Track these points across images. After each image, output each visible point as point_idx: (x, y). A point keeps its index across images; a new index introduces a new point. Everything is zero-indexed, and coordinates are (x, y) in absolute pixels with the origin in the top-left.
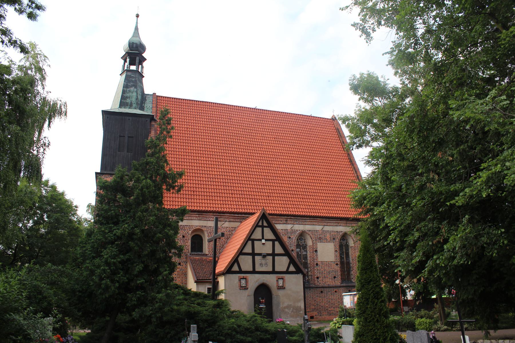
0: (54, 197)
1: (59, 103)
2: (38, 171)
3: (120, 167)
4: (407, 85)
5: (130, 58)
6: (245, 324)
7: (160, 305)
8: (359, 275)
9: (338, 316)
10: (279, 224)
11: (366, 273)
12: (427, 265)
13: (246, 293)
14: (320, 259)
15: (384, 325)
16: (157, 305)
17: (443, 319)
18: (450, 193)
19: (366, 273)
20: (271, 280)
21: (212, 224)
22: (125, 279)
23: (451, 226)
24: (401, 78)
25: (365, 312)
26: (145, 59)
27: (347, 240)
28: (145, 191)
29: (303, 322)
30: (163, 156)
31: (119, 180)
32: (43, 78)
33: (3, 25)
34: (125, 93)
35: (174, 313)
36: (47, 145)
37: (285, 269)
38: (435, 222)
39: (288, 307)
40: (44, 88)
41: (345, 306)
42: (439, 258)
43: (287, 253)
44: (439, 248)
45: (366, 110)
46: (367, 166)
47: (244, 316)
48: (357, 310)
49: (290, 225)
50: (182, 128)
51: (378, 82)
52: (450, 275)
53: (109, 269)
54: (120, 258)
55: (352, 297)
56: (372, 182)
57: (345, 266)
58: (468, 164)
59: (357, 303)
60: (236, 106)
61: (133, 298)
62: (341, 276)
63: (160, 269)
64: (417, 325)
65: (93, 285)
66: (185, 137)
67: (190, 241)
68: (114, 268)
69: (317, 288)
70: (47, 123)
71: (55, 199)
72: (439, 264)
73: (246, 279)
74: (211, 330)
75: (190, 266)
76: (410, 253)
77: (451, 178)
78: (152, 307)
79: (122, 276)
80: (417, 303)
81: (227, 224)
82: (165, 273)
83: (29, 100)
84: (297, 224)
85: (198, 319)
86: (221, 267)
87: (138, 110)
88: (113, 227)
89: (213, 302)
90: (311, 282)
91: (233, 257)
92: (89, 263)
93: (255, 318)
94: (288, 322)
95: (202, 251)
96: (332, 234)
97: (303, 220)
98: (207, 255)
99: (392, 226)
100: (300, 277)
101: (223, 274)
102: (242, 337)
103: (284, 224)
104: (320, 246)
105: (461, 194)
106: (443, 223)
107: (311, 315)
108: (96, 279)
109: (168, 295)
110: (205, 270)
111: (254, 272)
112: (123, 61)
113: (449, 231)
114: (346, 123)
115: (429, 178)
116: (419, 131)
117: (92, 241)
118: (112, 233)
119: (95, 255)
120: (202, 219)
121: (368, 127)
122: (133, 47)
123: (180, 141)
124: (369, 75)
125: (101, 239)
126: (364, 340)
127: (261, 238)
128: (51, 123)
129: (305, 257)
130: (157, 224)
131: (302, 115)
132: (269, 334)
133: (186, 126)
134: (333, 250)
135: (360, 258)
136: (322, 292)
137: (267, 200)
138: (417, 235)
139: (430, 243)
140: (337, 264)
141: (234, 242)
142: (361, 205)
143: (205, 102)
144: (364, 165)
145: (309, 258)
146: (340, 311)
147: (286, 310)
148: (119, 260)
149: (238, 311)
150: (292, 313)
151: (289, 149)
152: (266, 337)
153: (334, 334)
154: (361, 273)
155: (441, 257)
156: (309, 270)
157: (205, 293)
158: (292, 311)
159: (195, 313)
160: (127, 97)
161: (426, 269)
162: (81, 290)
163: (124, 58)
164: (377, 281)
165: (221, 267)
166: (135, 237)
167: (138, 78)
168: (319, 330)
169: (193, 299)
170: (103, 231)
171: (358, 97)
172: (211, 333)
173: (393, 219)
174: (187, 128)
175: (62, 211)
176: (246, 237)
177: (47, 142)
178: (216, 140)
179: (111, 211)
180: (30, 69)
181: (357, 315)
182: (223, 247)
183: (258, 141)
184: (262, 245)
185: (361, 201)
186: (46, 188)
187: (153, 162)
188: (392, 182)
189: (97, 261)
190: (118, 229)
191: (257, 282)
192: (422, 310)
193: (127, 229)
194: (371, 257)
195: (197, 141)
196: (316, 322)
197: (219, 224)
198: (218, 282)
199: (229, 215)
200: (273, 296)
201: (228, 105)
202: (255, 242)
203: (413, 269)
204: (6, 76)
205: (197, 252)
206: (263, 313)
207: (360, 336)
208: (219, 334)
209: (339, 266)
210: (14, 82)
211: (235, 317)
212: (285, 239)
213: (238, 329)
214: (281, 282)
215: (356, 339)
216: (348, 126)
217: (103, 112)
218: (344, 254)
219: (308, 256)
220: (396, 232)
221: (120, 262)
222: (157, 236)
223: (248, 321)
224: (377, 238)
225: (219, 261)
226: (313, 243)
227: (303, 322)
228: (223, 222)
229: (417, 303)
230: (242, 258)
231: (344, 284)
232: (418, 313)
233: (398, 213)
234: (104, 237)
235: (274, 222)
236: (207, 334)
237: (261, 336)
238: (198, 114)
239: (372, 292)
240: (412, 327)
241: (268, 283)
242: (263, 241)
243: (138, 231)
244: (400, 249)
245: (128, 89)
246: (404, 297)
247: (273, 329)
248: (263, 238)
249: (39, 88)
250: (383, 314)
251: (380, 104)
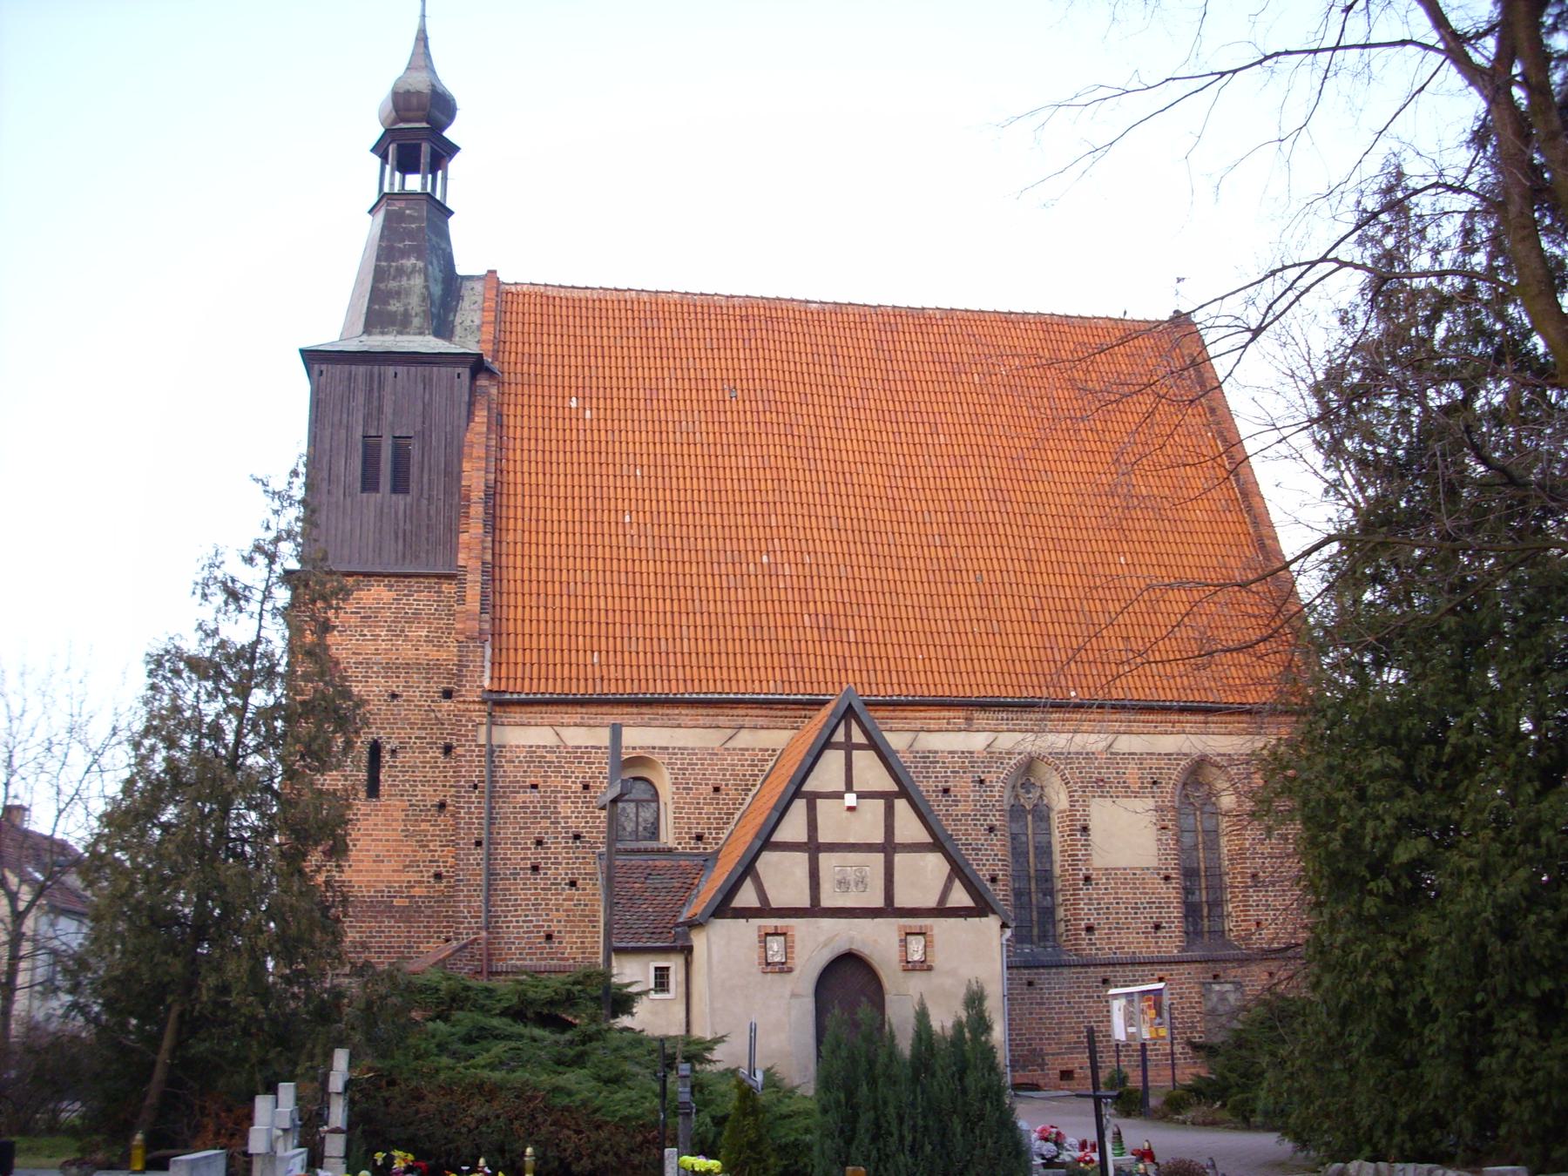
10: (940, 731)
13: (784, 985)
14: (1098, 861)
26: (453, 149)
37: (931, 901)
69: (1087, 965)
73: (784, 934)
87: (431, 338)
98: (670, 850)
107: (1064, 1068)
111: (815, 910)
120: (654, 723)
129: (1045, 851)
140: (1167, 878)
145: (1057, 857)
156: (1060, 899)
191: (825, 945)
200: (886, 997)
202: (819, 801)
214: (916, 949)
217: (312, 357)
219: (1057, 848)
226: (1073, 803)
231: (1196, 954)
242: (850, 799)
248: (849, 788)
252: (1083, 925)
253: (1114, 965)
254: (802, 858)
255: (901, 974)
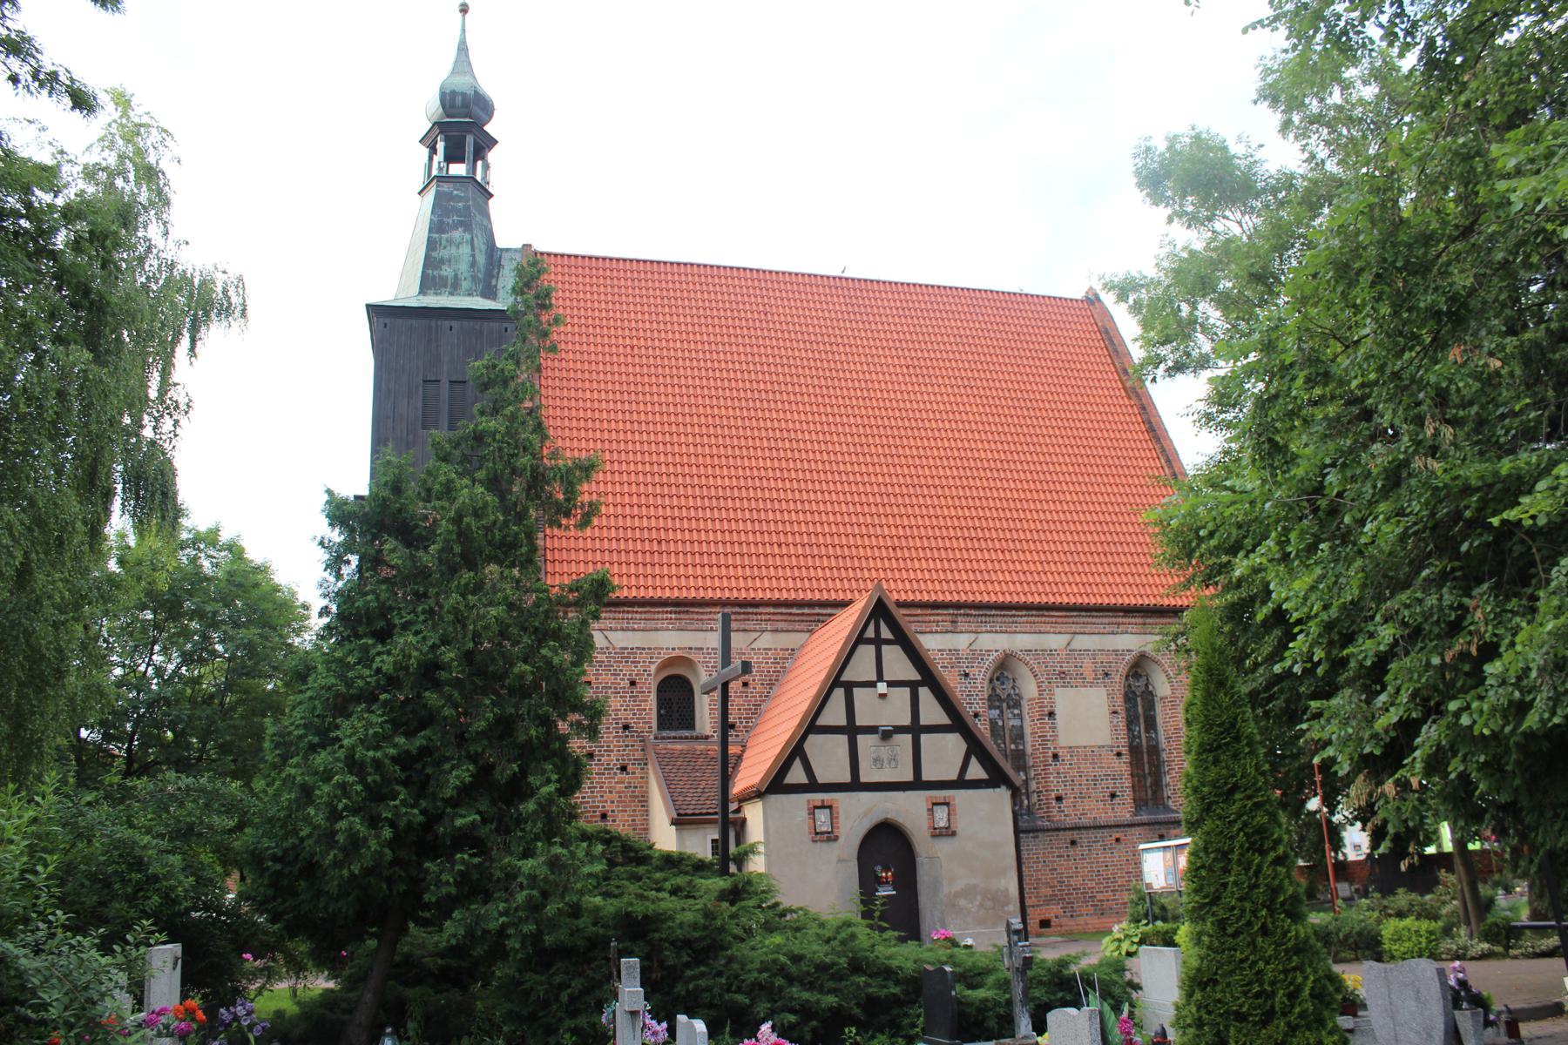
0: (238, 580)
1: (220, 280)
2: (164, 494)
3: (389, 451)
4: (1323, 162)
5: (447, 139)
6: (814, 953)
7: (530, 898)
8: (1191, 771)
9: (1128, 918)
10: (931, 632)
11: (1216, 762)
12: (1418, 741)
13: (833, 851)
15: (1290, 945)
16: (521, 897)
17: (1473, 920)
18: (1499, 486)
19: (1216, 762)
20: (909, 810)
21: (713, 640)
22: (414, 815)
23: (1508, 599)
24: (1304, 142)
25: (1219, 898)
27: (1147, 676)
28: (469, 525)
29: (1006, 939)
30: (531, 412)
31: (386, 493)
32: (162, 200)
33: (9, 23)
34: (434, 249)
35: (583, 922)
36: (183, 407)
37: (953, 775)
38: (1445, 590)
39: (968, 892)
40: (166, 234)
41: (1149, 886)
42: (1468, 707)
43: (958, 724)
44: (1471, 671)
45: (1192, 253)
46: (1205, 431)
47: (822, 925)
48: (1189, 894)
49: (966, 635)
50: (618, 347)
51: (1227, 159)
52: (1509, 768)
53: (358, 783)
54: (395, 746)
55: (1169, 855)
56: (1219, 475)
57: (1146, 760)
58: (1555, 389)
59: (1189, 870)
60: (784, 273)
61: (442, 875)
62: (1134, 791)
63: (531, 779)
64: (1385, 941)
65: (309, 836)
66: (628, 375)
67: (653, 697)
68: (378, 778)
69: (1058, 830)
70: (185, 342)
71: (240, 585)
72: (1471, 727)
73: (830, 807)
74: (703, 975)
75: (656, 773)
76: (1363, 697)
77: (1494, 439)
78: (506, 901)
79: (404, 803)
80: (1403, 868)
81: (767, 640)
82: (545, 790)
83: (118, 269)
84: (987, 632)
85: (661, 940)
86: (751, 773)
87: (479, 299)
88: (374, 645)
89: (720, 883)
90: (1040, 813)
91: (787, 743)
92: (297, 766)
93: (850, 930)
94: (969, 942)
95: (691, 726)
96: (1100, 658)
97: (1007, 619)
98: (707, 737)
99: (1297, 610)
100: (1003, 794)
101: (758, 794)
102: (806, 995)
103: (947, 632)
104: (1064, 700)
105: (1541, 485)
106: (1475, 592)
107: (1043, 917)
108: (316, 815)
109: (554, 863)
110: (704, 783)
111: (855, 785)
112: (426, 151)
113: (1498, 618)
114: (1131, 301)
115: (1420, 437)
116: (1378, 275)
117: (309, 694)
118: (369, 667)
119: (316, 740)
120: (690, 627)
121: (1200, 307)
122: (453, 106)
123: (610, 386)
124: (1197, 137)
125: (333, 685)
126: (1219, 1001)
127: (875, 679)
128: (199, 344)
129: (1019, 735)
130: (514, 631)
131: (992, 291)
132: (897, 983)
133: (628, 341)
134: (1106, 711)
135: (1195, 710)
136: (1073, 843)
137: (890, 559)
138: (1387, 633)
139: (1436, 661)
140: (1119, 754)
141: (789, 695)
142: (1190, 555)
143: (685, 264)
144: (1195, 430)
145: (1028, 738)
146: (1132, 901)
147: (962, 902)
148: (392, 751)
149: (801, 909)
150: (982, 911)
151: (935, 364)
152: (885, 991)
153: (1115, 977)
154: (1200, 765)
155: (1475, 705)
156: (1032, 774)
157: (700, 856)
158: (981, 905)
159: (646, 917)
160: (442, 261)
161: (1417, 754)
162: (280, 854)
163: (429, 142)
164: (1259, 790)
165: (751, 773)
166: (443, 675)
167: (474, 199)
168: (1063, 964)
169: (658, 875)
170: (341, 661)
171: (1163, 212)
172: (702, 983)
173: (1301, 584)
174: (632, 348)
175: (266, 623)
176: (827, 678)
177: (183, 401)
178: (740, 400)
179: (366, 594)
180: (119, 174)
181: (1187, 911)
182: (756, 711)
183: (855, 376)
184: (878, 701)
185: (1190, 542)
186: (211, 553)
187: (496, 431)
188: (1292, 460)
189: (321, 759)
190: (389, 653)
191: (865, 815)
192: (1401, 891)
193: (417, 649)
194: (1234, 703)
195: (666, 386)
196: (1059, 939)
197: (738, 641)
198: (744, 821)
199: (772, 610)
200: (919, 860)
201: (758, 271)
202: (855, 690)
203: (1377, 752)
204: (38, 192)
205: (678, 729)
206: (877, 914)
207: (1203, 985)
208: (730, 985)
209: (1126, 758)
210: (70, 214)
211: (791, 927)
212: (951, 679)
213: (793, 969)
214: (941, 816)
215: (1190, 995)
216: (1136, 308)
217: (375, 311)
218: (1142, 720)
219: (1028, 731)
220: (1314, 628)
221: (395, 760)
222: (516, 670)
223: (828, 941)
224: (1244, 660)
225: (745, 755)
226: (1041, 691)
227: (1004, 941)
228: (756, 635)
229: (1403, 868)
230: (814, 744)
231: (1144, 817)
232: (1385, 902)
233: (1316, 563)
234: (342, 677)
235: (913, 627)
236: (691, 987)
237: (871, 990)
238: (666, 301)
239: (1240, 830)
240: (1369, 947)
241: (901, 821)
242: (882, 687)
243: (452, 655)
244: (1327, 690)
245: (444, 236)
246: (1336, 853)
247: (909, 965)
249: (154, 232)
250: (1283, 904)
251: (1236, 230)
252: (1053, 795)
253: (1079, 828)
254: (843, 739)
255: (930, 839)
